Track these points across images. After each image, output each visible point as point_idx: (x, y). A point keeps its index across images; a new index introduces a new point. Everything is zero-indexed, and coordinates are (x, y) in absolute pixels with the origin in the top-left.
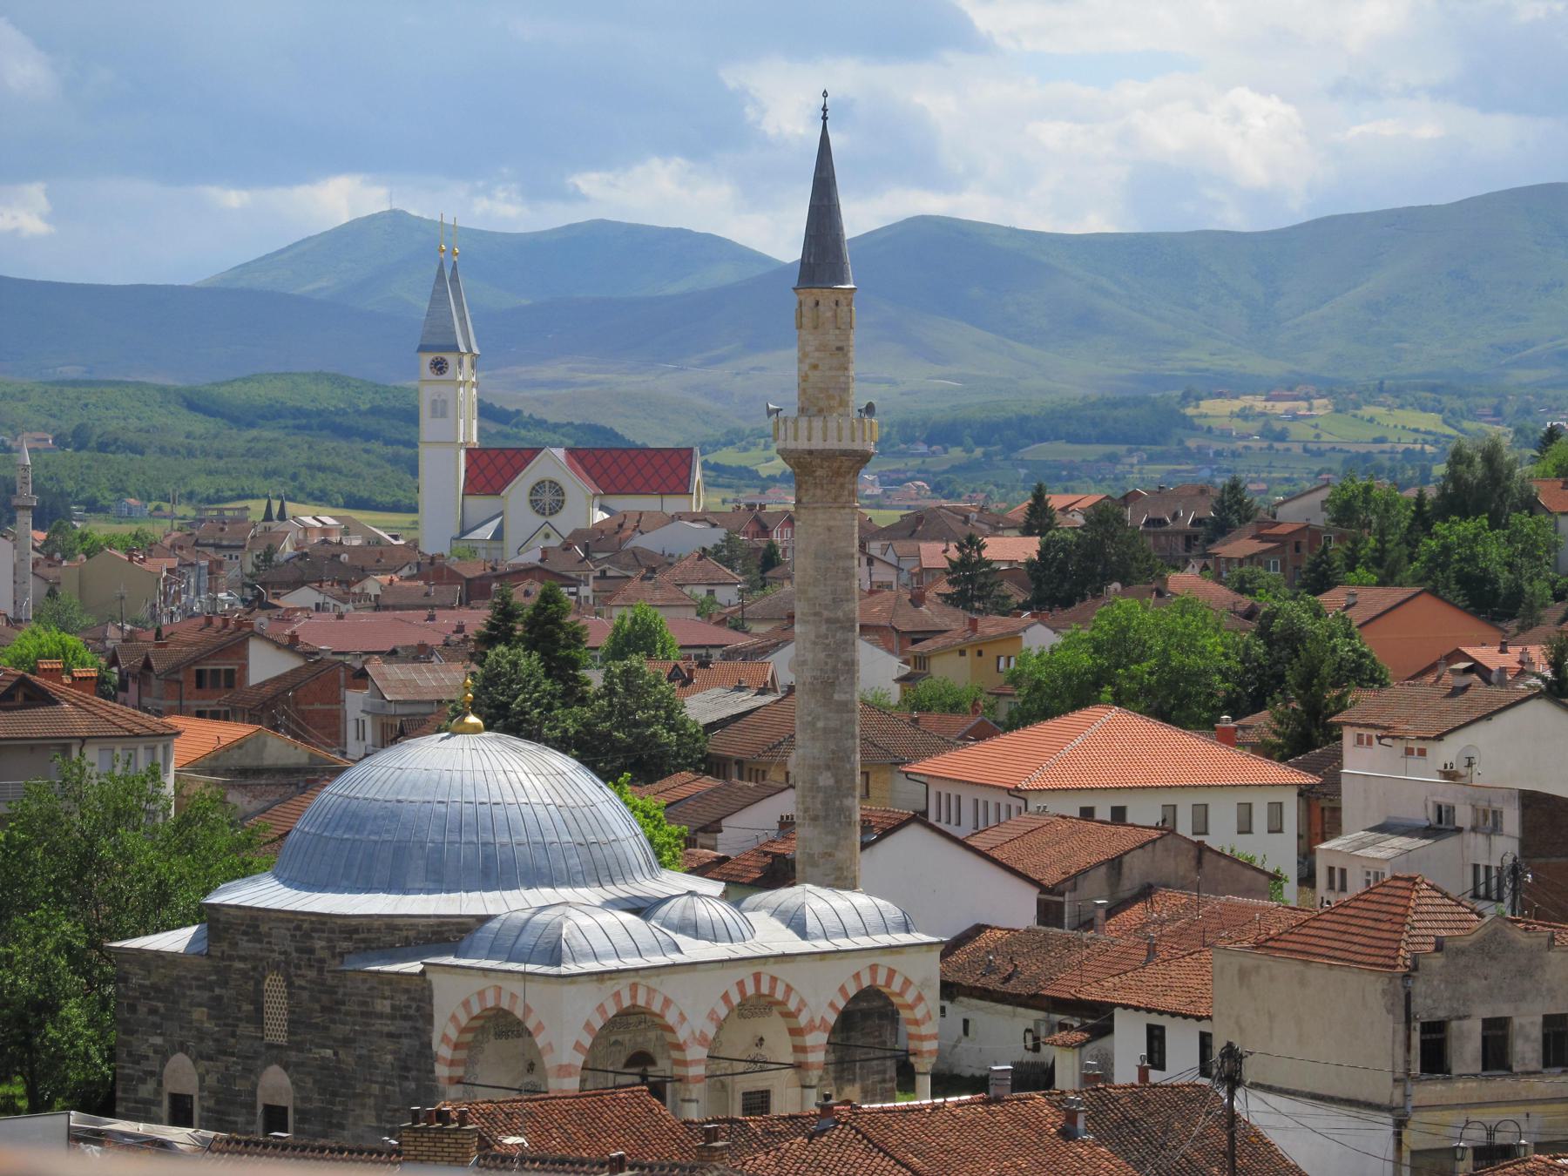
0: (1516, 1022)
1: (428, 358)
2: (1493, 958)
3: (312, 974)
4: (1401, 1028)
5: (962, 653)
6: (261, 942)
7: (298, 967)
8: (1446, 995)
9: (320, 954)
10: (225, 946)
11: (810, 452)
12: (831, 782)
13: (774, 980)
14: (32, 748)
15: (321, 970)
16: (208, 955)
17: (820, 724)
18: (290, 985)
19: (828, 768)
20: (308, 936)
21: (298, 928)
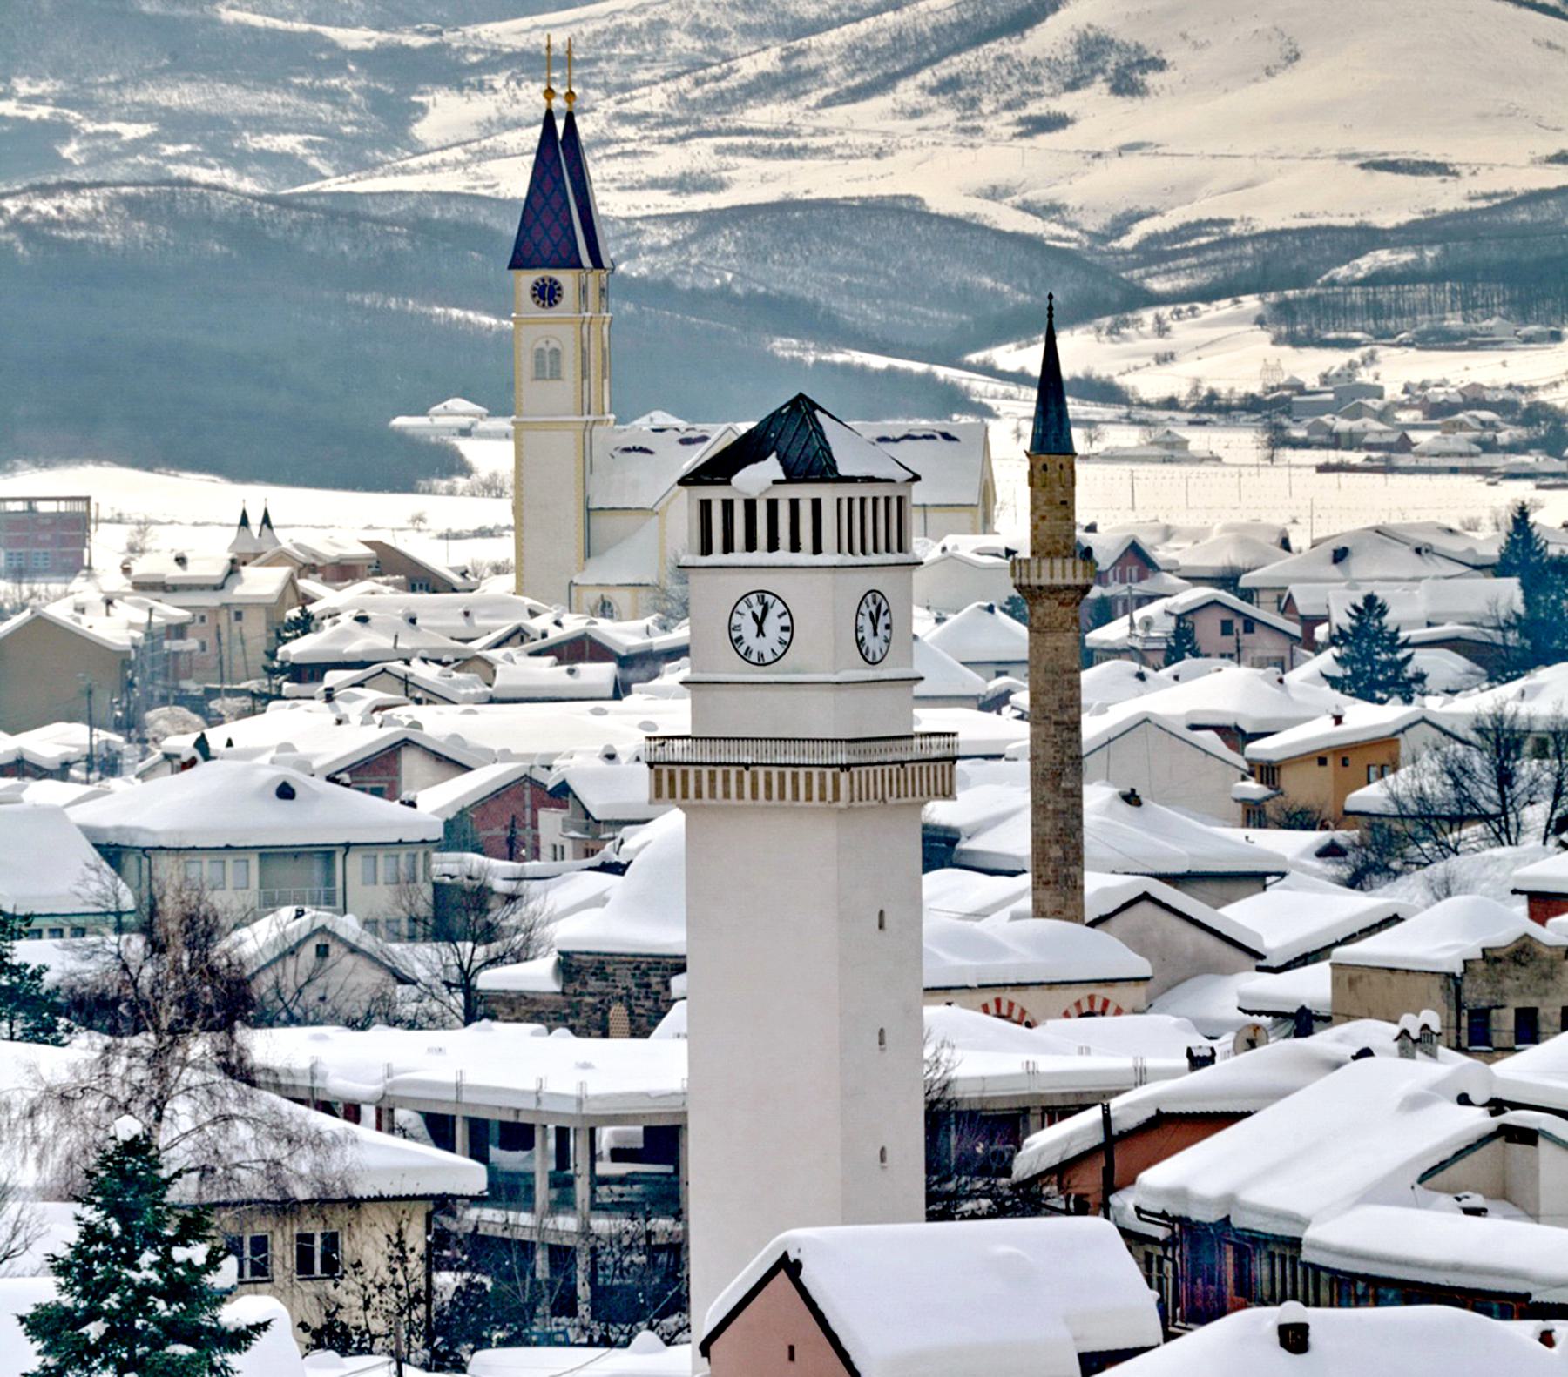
0: (1541, 1012)
1: (528, 279)
2: (1523, 965)
3: (649, 1004)
4: (1453, 1013)
5: (1322, 762)
6: (606, 980)
7: (638, 999)
8: (1488, 990)
9: (655, 988)
10: (577, 985)
11: (1040, 587)
12: (1060, 853)
13: (1011, 1004)
14: (296, 856)
15: (656, 1000)
16: (563, 993)
17: (1050, 807)
18: (631, 1013)
19: (1057, 842)
20: (645, 974)
21: (637, 968)
